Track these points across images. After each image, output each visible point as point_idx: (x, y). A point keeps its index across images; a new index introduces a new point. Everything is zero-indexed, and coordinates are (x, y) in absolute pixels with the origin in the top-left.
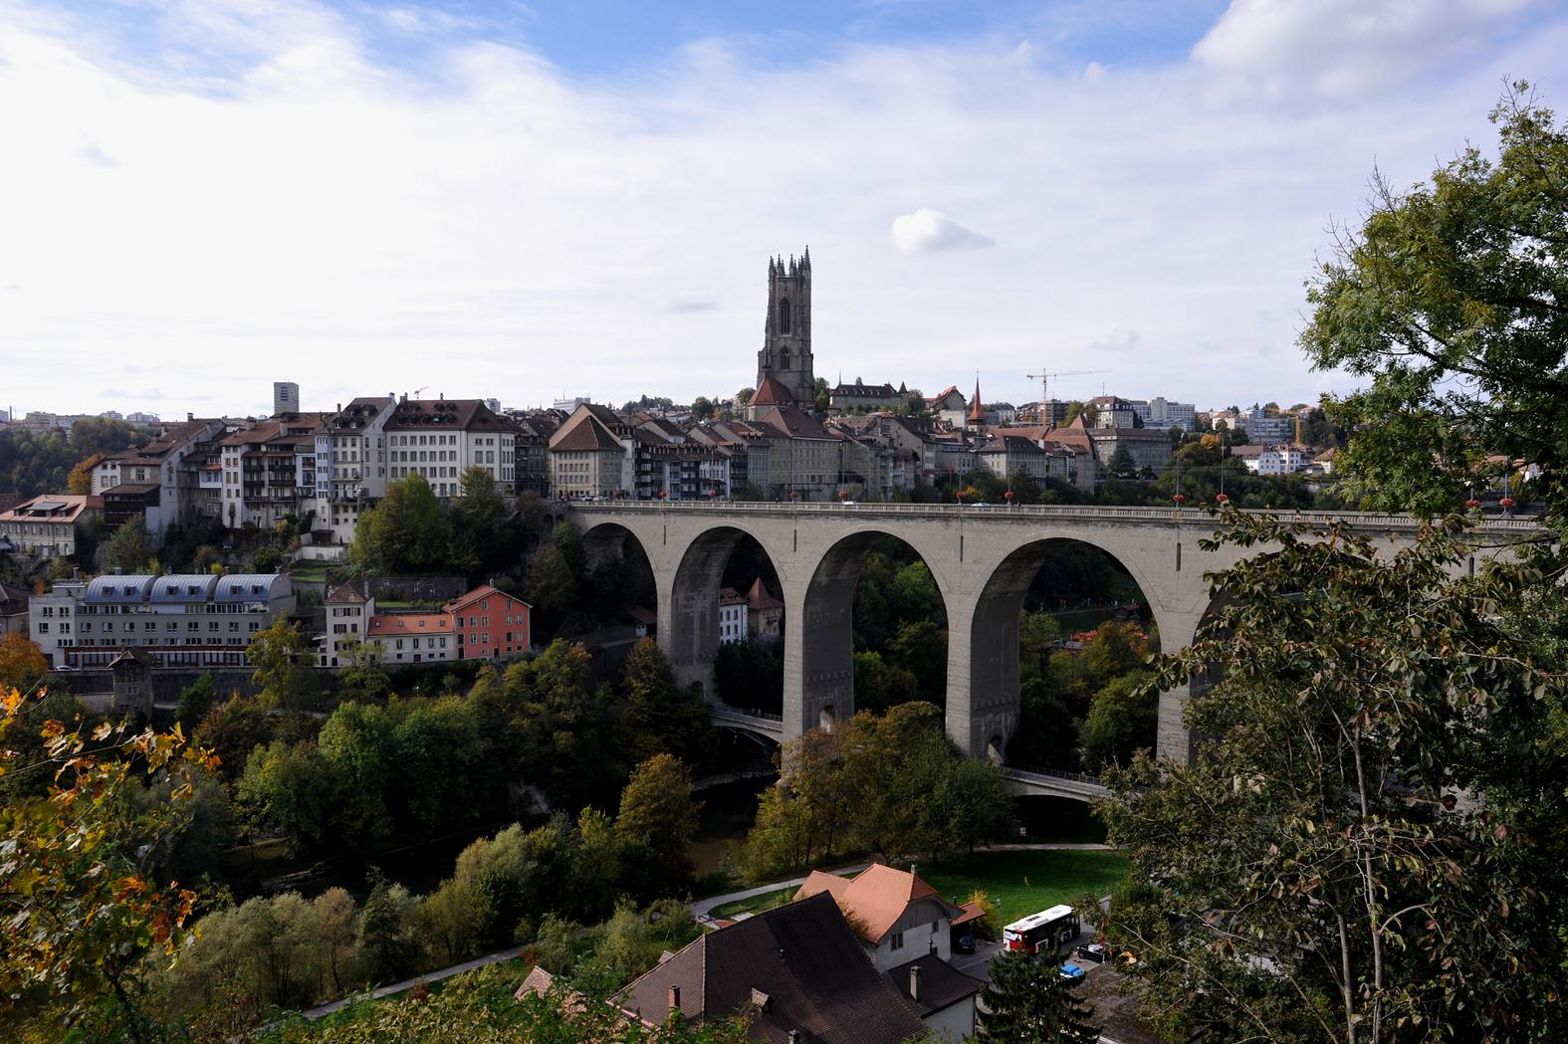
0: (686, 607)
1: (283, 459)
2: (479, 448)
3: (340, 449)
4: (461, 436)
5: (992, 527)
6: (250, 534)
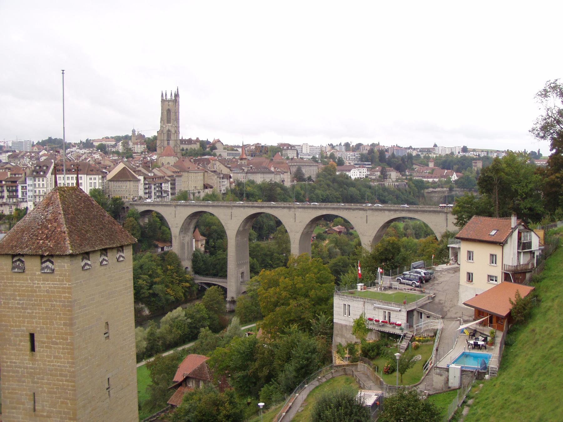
2: (91, 181)
3: (37, 182)
5: (306, 210)
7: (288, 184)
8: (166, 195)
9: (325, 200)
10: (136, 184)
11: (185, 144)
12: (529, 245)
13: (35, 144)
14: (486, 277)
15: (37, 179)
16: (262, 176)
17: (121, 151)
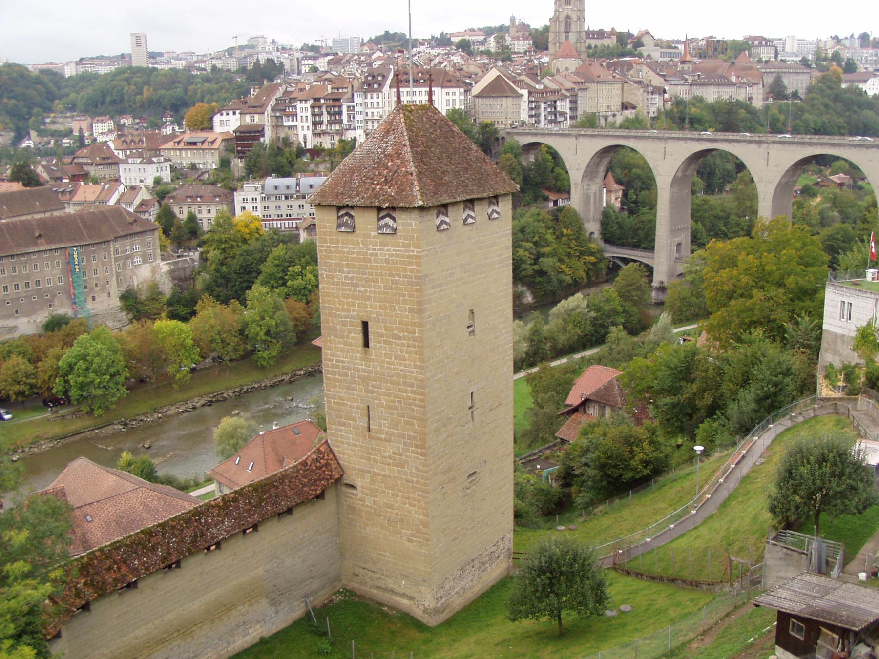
0: (588, 190)
1: (334, 107)
3: (369, 100)
6: (316, 152)
7: (758, 103)
8: (562, 119)
10: (516, 101)
11: (593, 38)
15: (369, 95)
16: (716, 89)
17: (493, 50)
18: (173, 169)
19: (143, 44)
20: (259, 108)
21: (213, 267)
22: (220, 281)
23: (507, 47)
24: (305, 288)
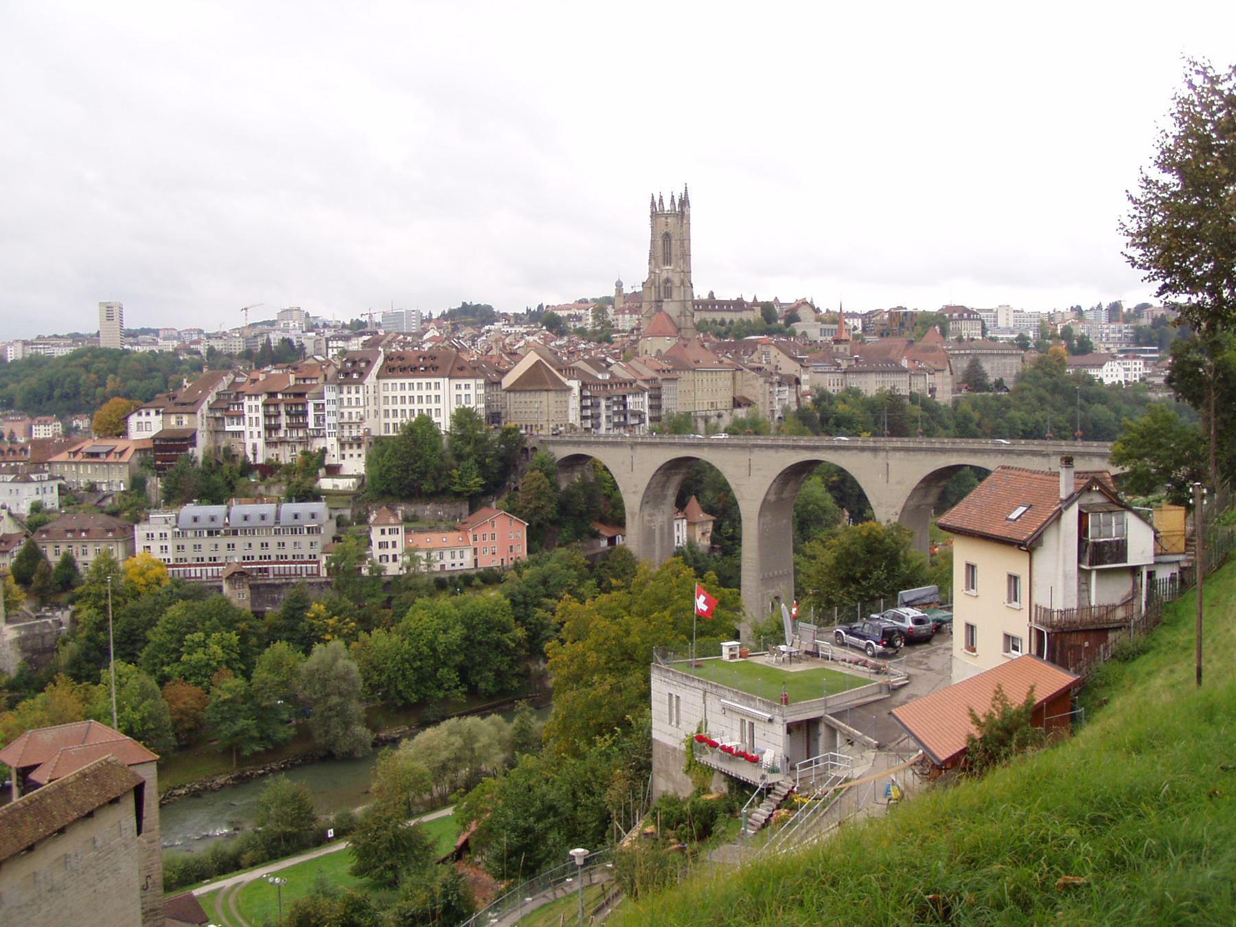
0: (650, 521)
1: (297, 405)
2: (459, 392)
3: (345, 396)
4: (444, 382)
5: (912, 456)
6: (268, 469)
7: (944, 396)
8: (637, 421)
9: (1031, 432)
10: (561, 397)
11: (728, 310)
12: (1119, 549)
13: (434, 317)
14: (1000, 641)
15: (345, 389)
16: (880, 378)
17: (589, 328)
18: (62, 490)
19: (116, 318)
20: (189, 406)
21: (84, 634)
22: (92, 654)
23: (609, 324)
24: (208, 665)
